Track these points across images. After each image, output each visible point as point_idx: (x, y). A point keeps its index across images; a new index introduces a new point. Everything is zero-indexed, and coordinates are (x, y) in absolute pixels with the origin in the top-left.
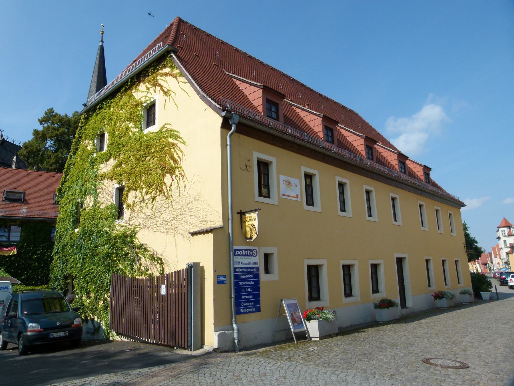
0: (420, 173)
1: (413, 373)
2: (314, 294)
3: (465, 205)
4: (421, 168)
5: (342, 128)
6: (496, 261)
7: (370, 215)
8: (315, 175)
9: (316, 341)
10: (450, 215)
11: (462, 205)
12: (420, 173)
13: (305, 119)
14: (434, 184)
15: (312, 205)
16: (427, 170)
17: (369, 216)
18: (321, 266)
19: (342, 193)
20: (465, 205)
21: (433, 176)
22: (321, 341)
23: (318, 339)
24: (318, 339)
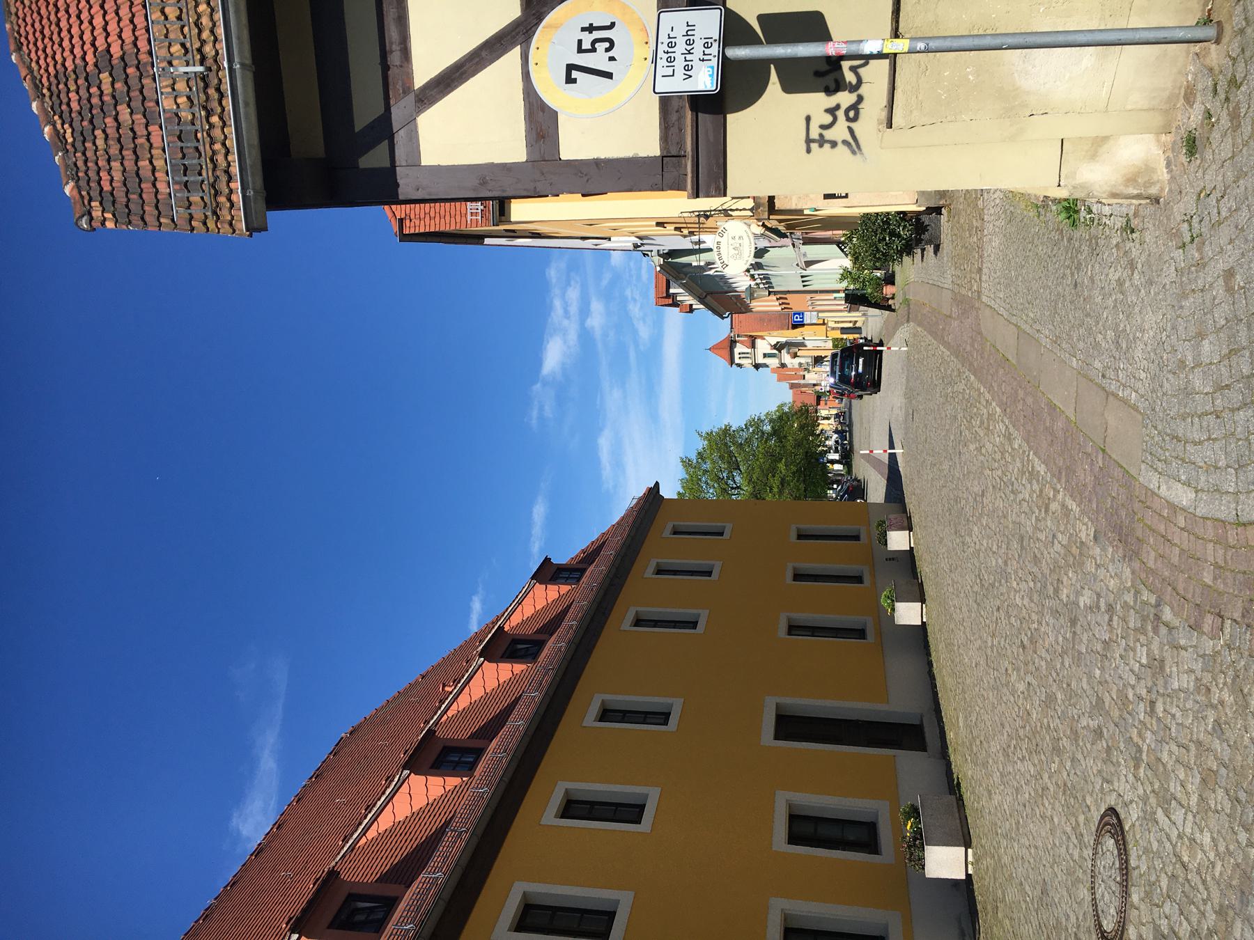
0: (547, 596)
1: (1160, 810)
2: (859, 835)
3: (657, 484)
4: (540, 588)
5: (364, 833)
6: (811, 378)
7: (664, 717)
8: (567, 791)
9: (974, 854)
10: (638, 622)
11: (654, 491)
12: (547, 596)
13: (400, 818)
14: (590, 556)
15: (641, 808)
16: (548, 573)
17: (695, 627)
18: (786, 917)
19: (625, 715)
20: (657, 484)
21: (562, 557)
22: (974, 844)
23: (970, 851)
24: (970, 851)
